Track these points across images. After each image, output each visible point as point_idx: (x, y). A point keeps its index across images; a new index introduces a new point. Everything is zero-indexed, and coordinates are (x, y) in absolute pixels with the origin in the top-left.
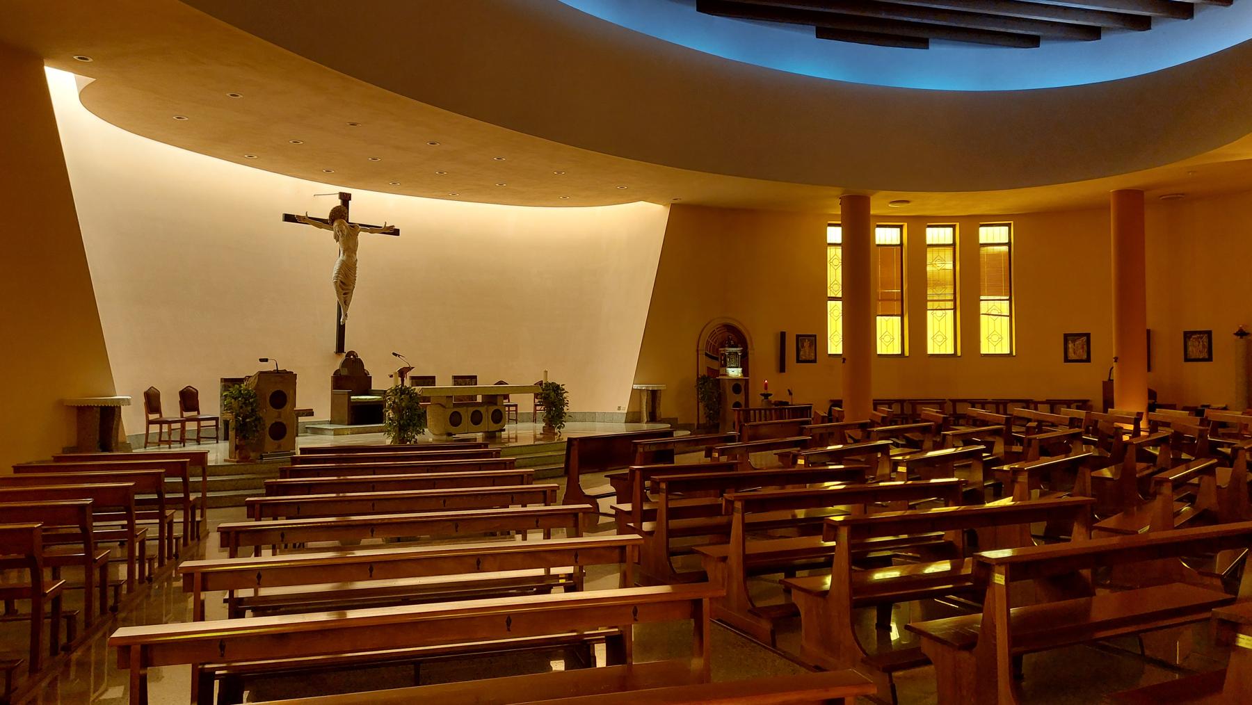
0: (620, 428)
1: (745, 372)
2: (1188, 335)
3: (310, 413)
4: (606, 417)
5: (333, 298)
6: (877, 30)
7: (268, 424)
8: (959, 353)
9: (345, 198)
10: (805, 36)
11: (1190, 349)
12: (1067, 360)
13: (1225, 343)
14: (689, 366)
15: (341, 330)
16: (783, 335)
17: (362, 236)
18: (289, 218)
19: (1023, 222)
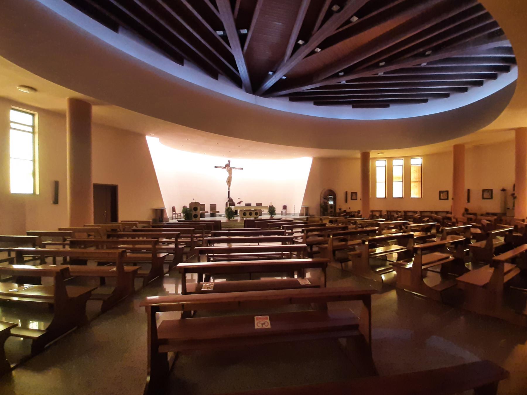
0: (298, 217)
1: (335, 203)
2: (484, 191)
3: (219, 212)
4: (295, 214)
5: (227, 186)
6: (372, 104)
7: (193, 215)
8: (38, 193)
9: (229, 161)
10: (349, 108)
11: (484, 195)
12: (440, 199)
13: (497, 193)
14: (317, 200)
15: (229, 192)
16: (346, 192)
17: (233, 170)
18: (216, 167)
19: (427, 157)
